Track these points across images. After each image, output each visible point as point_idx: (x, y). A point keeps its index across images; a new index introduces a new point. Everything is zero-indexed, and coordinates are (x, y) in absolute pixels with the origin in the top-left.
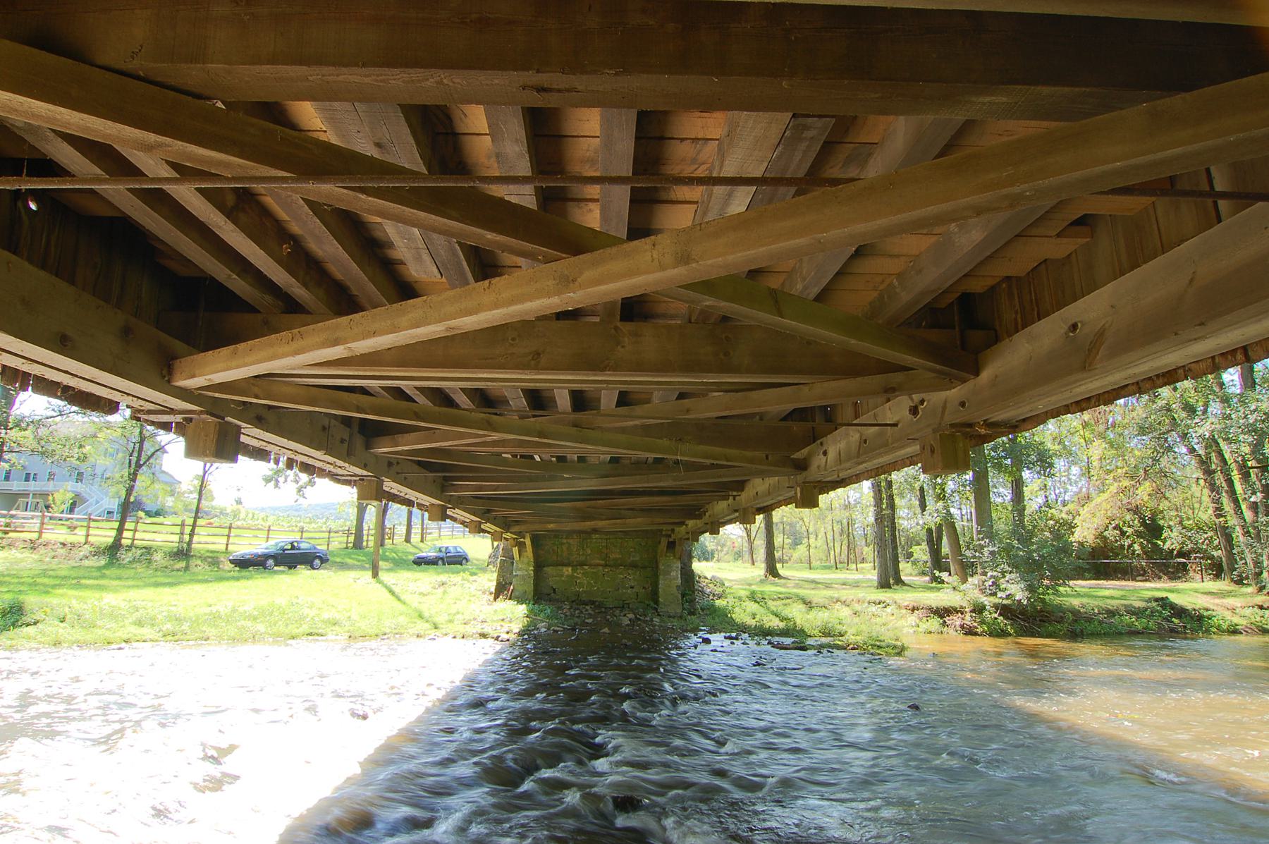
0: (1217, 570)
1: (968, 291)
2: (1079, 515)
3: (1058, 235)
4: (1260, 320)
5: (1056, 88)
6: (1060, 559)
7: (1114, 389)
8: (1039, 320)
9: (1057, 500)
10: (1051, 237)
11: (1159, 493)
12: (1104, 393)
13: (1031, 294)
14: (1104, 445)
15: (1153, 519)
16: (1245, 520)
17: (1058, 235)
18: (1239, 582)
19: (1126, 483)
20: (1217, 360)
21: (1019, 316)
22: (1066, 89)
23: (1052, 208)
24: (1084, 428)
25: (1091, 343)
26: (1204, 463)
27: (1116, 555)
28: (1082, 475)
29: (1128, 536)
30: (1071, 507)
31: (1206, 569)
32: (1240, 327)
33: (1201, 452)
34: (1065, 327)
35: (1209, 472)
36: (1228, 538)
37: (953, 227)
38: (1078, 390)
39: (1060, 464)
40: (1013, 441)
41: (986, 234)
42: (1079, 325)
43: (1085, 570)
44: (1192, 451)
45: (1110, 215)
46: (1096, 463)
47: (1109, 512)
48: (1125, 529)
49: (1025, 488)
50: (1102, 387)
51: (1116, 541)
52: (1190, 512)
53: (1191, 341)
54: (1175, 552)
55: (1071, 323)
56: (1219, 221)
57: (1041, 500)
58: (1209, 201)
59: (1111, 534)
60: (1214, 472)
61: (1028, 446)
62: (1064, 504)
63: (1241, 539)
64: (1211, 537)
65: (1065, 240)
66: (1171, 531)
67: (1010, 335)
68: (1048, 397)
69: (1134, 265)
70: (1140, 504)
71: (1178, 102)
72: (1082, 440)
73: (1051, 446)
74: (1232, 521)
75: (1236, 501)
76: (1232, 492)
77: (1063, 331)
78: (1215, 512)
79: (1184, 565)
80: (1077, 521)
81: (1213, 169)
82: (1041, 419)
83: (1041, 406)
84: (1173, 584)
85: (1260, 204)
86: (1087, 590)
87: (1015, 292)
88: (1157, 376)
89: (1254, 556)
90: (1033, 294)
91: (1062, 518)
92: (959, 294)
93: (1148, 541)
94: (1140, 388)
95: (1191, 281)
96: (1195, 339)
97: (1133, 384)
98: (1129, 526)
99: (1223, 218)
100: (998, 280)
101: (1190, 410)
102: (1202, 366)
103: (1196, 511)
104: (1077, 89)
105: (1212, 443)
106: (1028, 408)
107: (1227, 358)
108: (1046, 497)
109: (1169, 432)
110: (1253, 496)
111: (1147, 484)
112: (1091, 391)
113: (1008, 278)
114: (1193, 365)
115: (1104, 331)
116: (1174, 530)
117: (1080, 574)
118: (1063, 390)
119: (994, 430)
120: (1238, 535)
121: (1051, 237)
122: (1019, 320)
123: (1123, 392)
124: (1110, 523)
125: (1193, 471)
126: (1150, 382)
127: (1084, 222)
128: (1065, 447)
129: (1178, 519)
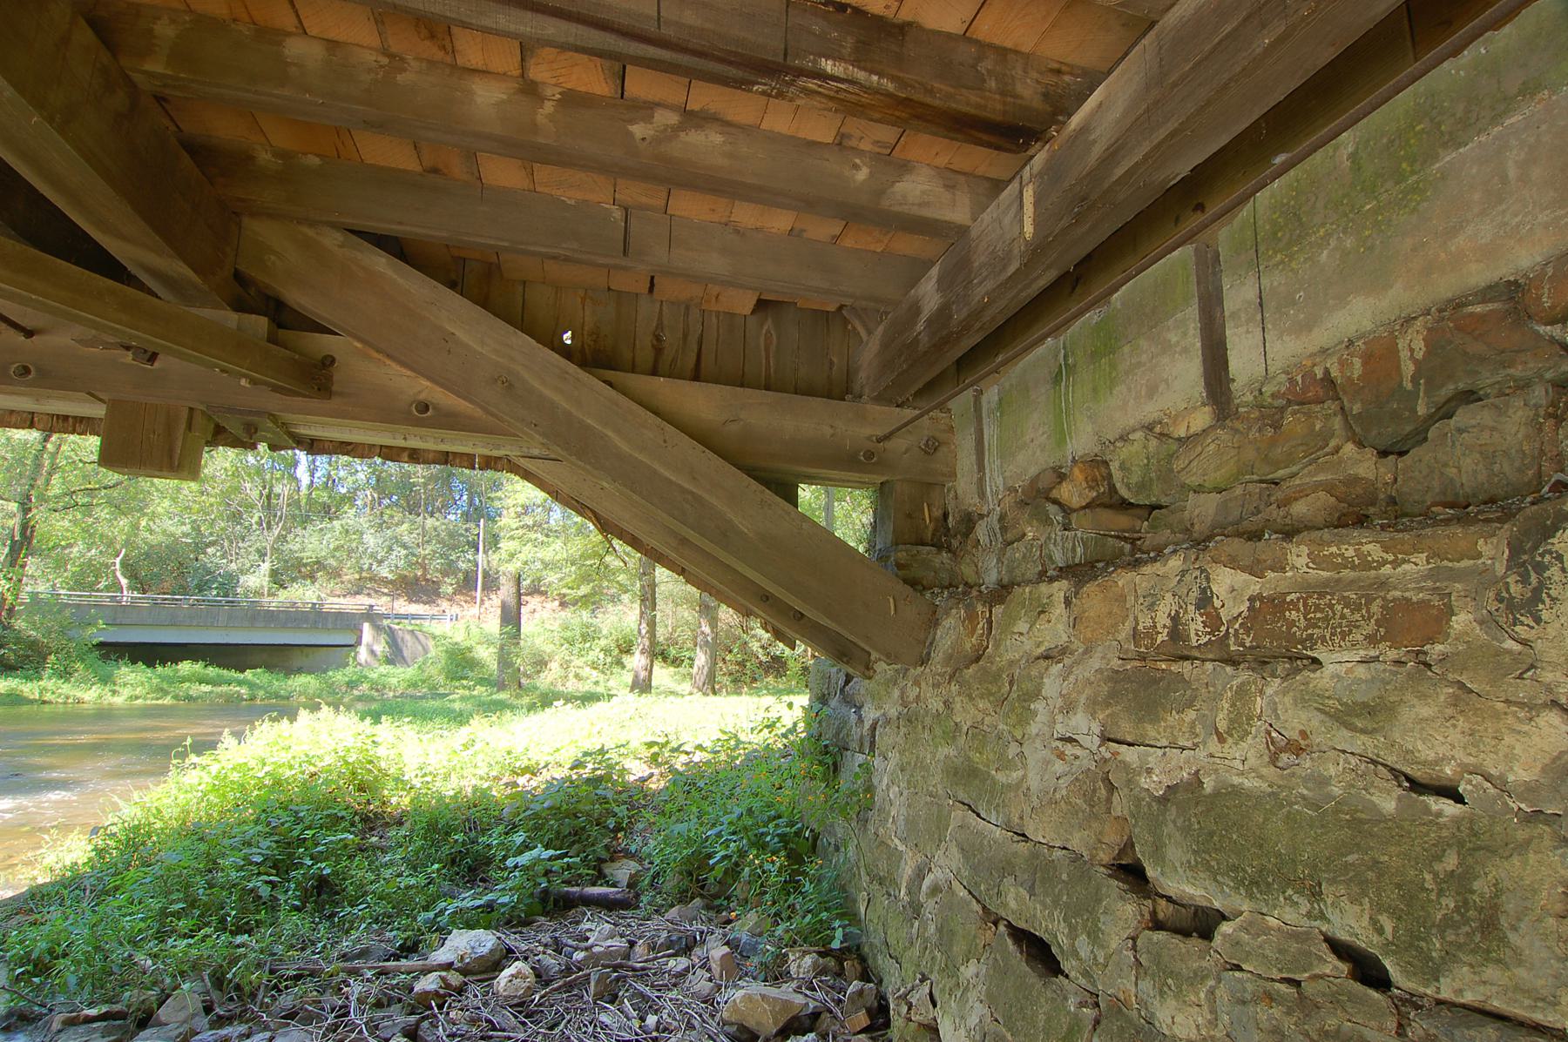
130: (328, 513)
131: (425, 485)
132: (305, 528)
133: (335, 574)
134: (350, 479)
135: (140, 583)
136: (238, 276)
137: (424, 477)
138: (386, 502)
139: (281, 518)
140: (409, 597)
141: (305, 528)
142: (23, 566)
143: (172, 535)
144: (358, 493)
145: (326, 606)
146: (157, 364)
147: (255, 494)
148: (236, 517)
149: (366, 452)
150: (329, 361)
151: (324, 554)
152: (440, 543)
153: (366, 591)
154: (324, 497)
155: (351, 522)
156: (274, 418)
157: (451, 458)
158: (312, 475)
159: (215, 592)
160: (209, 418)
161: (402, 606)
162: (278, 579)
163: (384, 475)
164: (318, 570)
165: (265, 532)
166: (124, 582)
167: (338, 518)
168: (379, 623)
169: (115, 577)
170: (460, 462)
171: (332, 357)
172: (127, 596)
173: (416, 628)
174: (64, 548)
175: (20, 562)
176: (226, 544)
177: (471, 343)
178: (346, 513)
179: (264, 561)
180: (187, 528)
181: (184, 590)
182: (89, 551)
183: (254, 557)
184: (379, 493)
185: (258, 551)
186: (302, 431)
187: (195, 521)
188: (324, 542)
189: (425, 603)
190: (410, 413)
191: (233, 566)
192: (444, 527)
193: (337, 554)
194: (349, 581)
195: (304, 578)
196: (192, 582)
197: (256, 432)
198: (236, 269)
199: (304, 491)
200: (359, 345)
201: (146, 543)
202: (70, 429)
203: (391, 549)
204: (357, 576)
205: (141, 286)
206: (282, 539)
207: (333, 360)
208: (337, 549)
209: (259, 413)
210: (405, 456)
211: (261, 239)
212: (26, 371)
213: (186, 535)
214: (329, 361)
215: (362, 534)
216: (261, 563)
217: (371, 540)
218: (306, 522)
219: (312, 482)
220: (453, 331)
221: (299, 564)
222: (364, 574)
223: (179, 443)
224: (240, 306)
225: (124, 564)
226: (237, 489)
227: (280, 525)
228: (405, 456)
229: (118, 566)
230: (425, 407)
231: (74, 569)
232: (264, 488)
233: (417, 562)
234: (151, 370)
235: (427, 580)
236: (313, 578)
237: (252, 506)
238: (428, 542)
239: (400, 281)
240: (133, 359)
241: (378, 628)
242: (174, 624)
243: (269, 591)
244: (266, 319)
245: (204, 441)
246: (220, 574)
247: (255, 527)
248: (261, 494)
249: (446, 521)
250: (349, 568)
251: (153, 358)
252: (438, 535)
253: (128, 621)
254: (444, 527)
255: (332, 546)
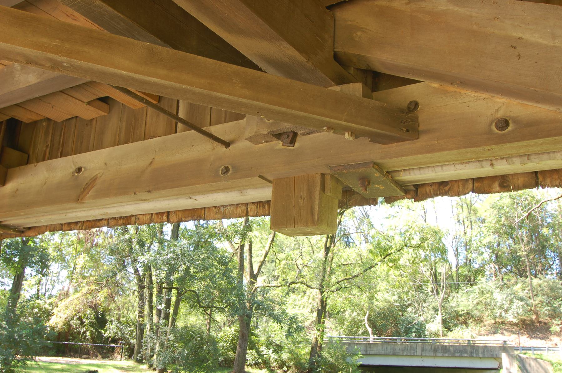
0: (130, 353)
1: (16, 118)
2: (57, 307)
3: (89, 103)
4: (178, 198)
5: (104, 5)
6: (34, 339)
7: (93, 220)
8: (61, 156)
9: (45, 294)
10: (84, 102)
11: (111, 298)
12: (88, 221)
13: (60, 138)
14: (87, 258)
15: (103, 315)
16: (153, 321)
17: (89, 103)
18: (140, 362)
19: (93, 287)
20: (153, 217)
21: (48, 150)
22: (110, 9)
23: (87, 82)
24: (77, 243)
25: (87, 184)
26: (141, 280)
27: (74, 338)
28: (68, 277)
29: (85, 325)
30: (53, 300)
31: (125, 352)
32: (168, 200)
33: (141, 273)
34: (74, 168)
35: (142, 287)
36: (142, 331)
37: (17, 66)
38: (73, 215)
39: (54, 267)
40: (25, 243)
41: (39, 80)
42: (83, 169)
43: (50, 349)
44: (136, 271)
45: (123, 104)
46: (78, 270)
47: (78, 306)
48: (84, 320)
49: (23, 282)
50: (86, 217)
51: (77, 328)
52: (126, 312)
53: (142, 200)
54: (110, 339)
55: (78, 166)
56: (176, 132)
57: (34, 292)
58: (174, 121)
59: (75, 323)
60: (144, 287)
61: (35, 249)
62: (50, 297)
63: (148, 333)
64: (133, 331)
65: (92, 108)
66: (112, 324)
67: (38, 161)
68: (50, 215)
69: (126, 142)
70: (98, 303)
71: (166, 51)
72: (74, 252)
73: (51, 252)
74: (147, 321)
75: (151, 308)
76: (151, 301)
77: (71, 170)
78: (139, 314)
79: (113, 348)
80: (55, 311)
81: (181, 102)
82: (40, 230)
83: (43, 221)
84: (103, 361)
85: (193, 131)
86: (47, 364)
87: (51, 131)
88: (120, 218)
89: (152, 344)
90: (62, 138)
91: (45, 308)
92: (8, 118)
93: (96, 330)
94: (109, 223)
95: (151, 163)
96: (144, 200)
97: (106, 219)
98: (87, 319)
99: (178, 131)
100: (40, 118)
101: (141, 244)
102: (146, 218)
103: (129, 312)
104: (116, 12)
105: (148, 268)
106: (34, 220)
107: (158, 217)
108: (38, 290)
109: (127, 256)
110: (160, 306)
111: (106, 290)
112: (79, 218)
113: (48, 120)
114: (141, 216)
115: (97, 178)
116: (114, 323)
117: (45, 351)
118: (61, 212)
119: (4, 231)
120: (147, 331)
121: (84, 102)
122: (48, 153)
123: (98, 224)
124: (76, 315)
125: (134, 285)
126: (115, 221)
127: (105, 100)
128: (61, 255)
129: (118, 316)
130: (470, 281)
131: (528, 256)
132: (458, 292)
133: (479, 320)
134: (480, 258)
135: (378, 331)
136: (336, 57)
137: (526, 251)
138: (504, 270)
139: (443, 287)
140: (529, 335)
141: (458, 292)
142: (323, 323)
143: (389, 302)
144: (486, 267)
145: (477, 342)
146: (297, 145)
147: (428, 274)
148: (419, 288)
149: (461, 189)
150: (414, 106)
151: (470, 308)
152: (544, 295)
153: (500, 331)
154: (464, 271)
155: (484, 286)
156: (378, 166)
157: (540, 179)
158: (457, 258)
159: (414, 335)
160: (338, 181)
161: (525, 340)
162: (447, 325)
163: (500, 253)
164: (470, 319)
165: (436, 296)
166: (370, 330)
167: (476, 284)
168: (512, 353)
169: (365, 327)
170: (551, 182)
171: (415, 101)
172: (372, 338)
173: (538, 357)
174: (343, 313)
175: (322, 320)
176: (416, 305)
177: (541, 41)
178: (480, 280)
179: (437, 314)
180: (396, 298)
181: (398, 334)
182: (353, 313)
183: (432, 312)
184: (498, 265)
185: (434, 308)
186: (405, 177)
187: (399, 293)
188: (470, 300)
189: (542, 339)
190: (490, 132)
191: (422, 319)
192: (546, 284)
193: (479, 307)
194: (489, 325)
195: (461, 324)
196: (402, 328)
197: (369, 184)
198: (334, 52)
199: (454, 269)
200: (435, 85)
201: (377, 307)
202: (267, 212)
203: (511, 301)
204: (493, 321)
205: (256, 67)
206: (446, 300)
207: (416, 104)
208: (478, 304)
209: (365, 164)
210: (496, 186)
211: (349, 23)
212: (227, 170)
213: (396, 301)
214: (414, 106)
215: (492, 293)
216: (436, 316)
217: (499, 297)
218: (458, 288)
219: (458, 262)
220: (518, 35)
221: (458, 315)
222: (497, 320)
223: (317, 203)
224: (341, 80)
225: (369, 319)
226: (416, 272)
227: (444, 291)
228: (496, 186)
229: (366, 321)
230: (504, 123)
231: (347, 324)
232: (432, 269)
233: (531, 310)
234: (293, 150)
235: (540, 322)
236: (466, 323)
237: (427, 281)
238: (536, 295)
239: (462, 10)
240: (283, 145)
241: (512, 357)
242: (395, 354)
243: (443, 333)
244: (361, 84)
245: (337, 202)
246: (415, 323)
247: (430, 294)
248: (431, 273)
249: (546, 280)
250: (488, 316)
251: (293, 138)
252: (542, 290)
253: (372, 352)
254: (546, 284)
255: (475, 302)
